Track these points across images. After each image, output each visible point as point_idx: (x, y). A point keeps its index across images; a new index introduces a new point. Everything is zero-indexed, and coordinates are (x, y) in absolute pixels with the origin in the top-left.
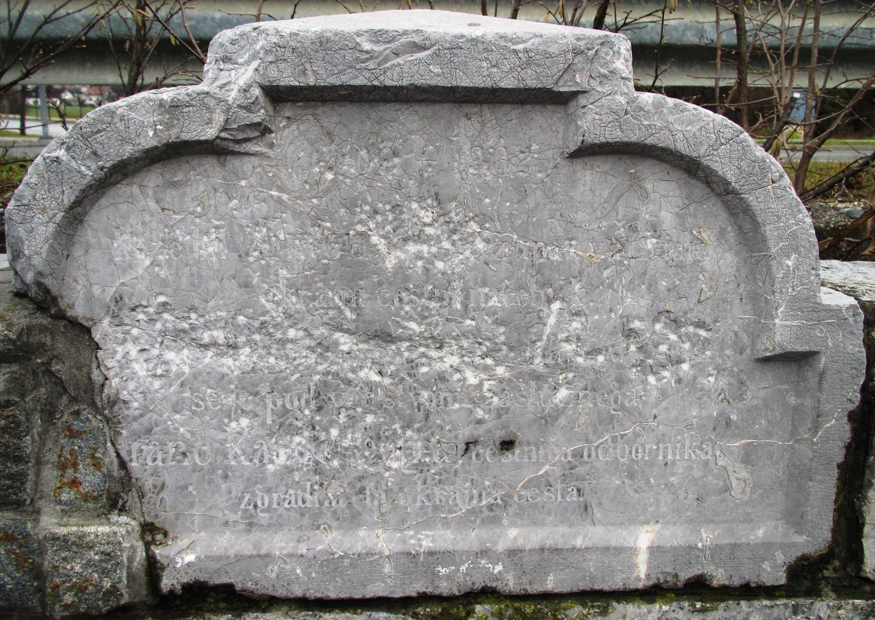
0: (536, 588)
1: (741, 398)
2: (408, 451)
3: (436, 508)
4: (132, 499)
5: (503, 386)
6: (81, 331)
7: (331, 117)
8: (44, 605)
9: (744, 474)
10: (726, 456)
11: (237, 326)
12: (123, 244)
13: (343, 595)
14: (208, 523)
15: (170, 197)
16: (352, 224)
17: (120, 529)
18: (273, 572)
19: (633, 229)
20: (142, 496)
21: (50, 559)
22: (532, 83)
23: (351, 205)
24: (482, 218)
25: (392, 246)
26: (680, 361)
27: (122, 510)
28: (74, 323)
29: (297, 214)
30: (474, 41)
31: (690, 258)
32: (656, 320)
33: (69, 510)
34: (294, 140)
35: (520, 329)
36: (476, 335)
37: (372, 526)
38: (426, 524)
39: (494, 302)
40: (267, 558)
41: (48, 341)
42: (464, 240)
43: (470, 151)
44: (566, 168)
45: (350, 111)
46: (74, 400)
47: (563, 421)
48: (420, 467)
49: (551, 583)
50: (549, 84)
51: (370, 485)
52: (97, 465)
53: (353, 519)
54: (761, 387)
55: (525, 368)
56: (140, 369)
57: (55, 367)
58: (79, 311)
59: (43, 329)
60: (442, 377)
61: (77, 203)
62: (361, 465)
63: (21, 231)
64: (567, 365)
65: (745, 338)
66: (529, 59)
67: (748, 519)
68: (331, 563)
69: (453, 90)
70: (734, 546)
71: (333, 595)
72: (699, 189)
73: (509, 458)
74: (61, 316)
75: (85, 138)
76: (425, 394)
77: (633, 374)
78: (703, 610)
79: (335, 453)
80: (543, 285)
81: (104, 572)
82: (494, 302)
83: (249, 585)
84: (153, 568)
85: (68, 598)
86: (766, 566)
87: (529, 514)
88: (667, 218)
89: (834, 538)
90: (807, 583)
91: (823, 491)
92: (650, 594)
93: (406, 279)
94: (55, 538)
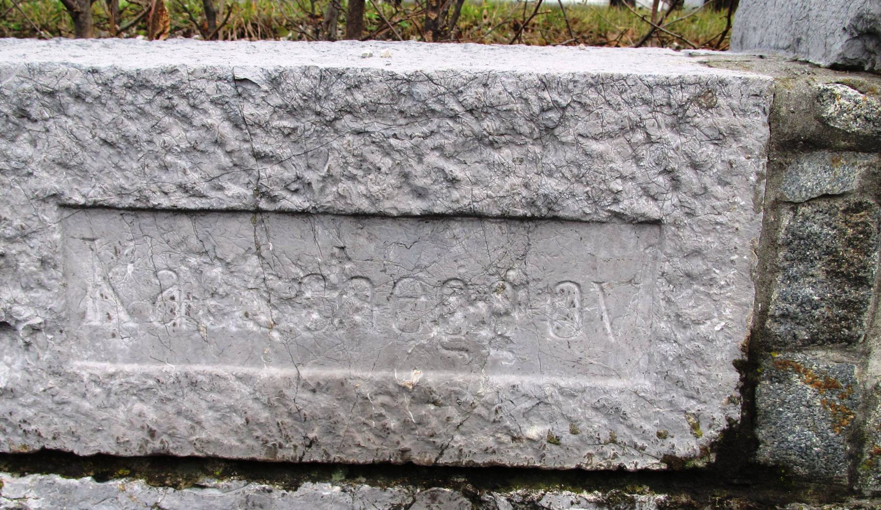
8: (853, 476)
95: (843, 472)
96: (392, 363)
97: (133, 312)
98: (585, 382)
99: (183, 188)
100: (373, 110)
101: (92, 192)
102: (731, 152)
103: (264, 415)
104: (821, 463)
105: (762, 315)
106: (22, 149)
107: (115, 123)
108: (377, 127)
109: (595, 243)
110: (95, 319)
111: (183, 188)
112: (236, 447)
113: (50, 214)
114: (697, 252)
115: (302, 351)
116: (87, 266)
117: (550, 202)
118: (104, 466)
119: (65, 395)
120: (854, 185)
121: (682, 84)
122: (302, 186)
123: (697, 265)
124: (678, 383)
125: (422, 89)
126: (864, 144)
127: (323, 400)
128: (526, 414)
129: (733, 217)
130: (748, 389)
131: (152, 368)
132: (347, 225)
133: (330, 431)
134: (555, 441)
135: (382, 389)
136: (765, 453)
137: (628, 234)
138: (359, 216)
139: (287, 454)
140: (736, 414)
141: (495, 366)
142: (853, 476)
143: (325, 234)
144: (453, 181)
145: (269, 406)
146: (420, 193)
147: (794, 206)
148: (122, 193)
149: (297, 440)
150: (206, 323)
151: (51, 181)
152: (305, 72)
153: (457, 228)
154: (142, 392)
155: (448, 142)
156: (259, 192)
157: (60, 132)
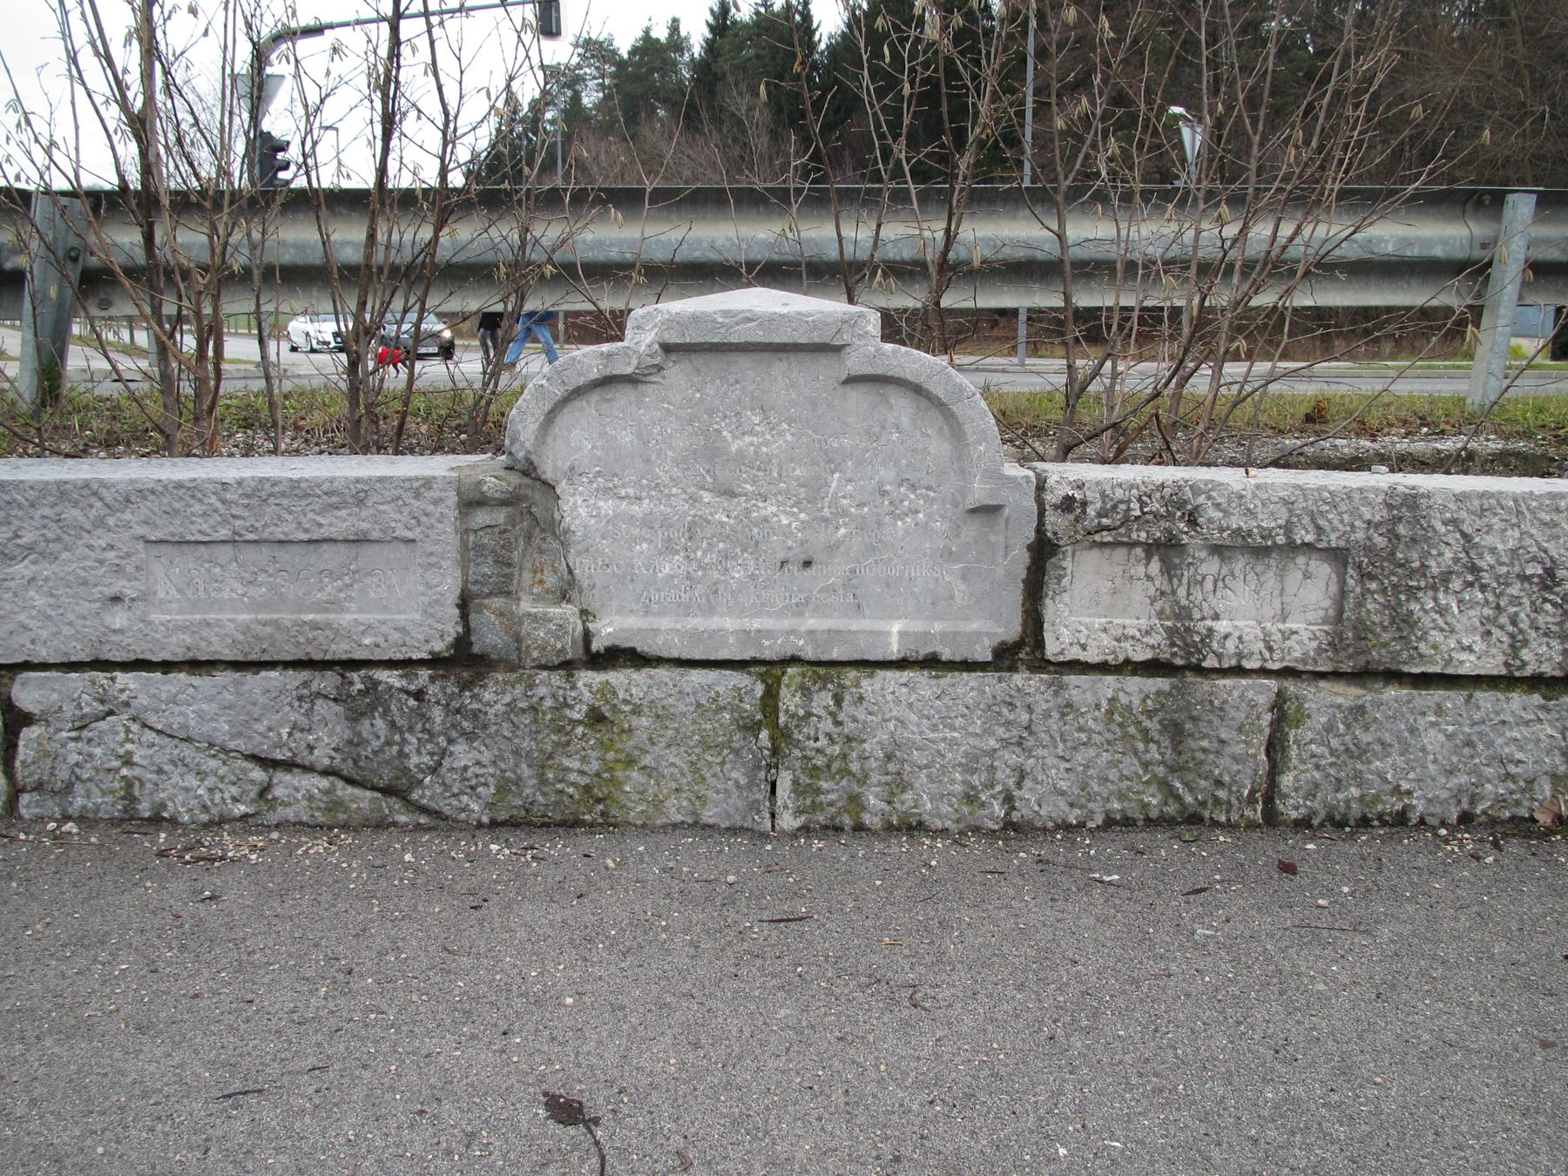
0: (825, 658)
1: (958, 536)
2: (744, 566)
3: (763, 604)
4: (574, 594)
5: (804, 526)
6: (549, 487)
7: (699, 360)
8: (520, 659)
9: (963, 587)
10: (950, 575)
11: (641, 486)
12: (576, 435)
13: (704, 657)
14: (621, 611)
15: (604, 407)
16: (711, 425)
17: (568, 611)
18: (660, 640)
19: (883, 427)
20: (581, 592)
21: (526, 627)
22: (817, 340)
23: (711, 412)
24: (790, 420)
25: (734, 437)
26: (917, 512)
27: (568, 601)
28: (545, 483)
29: (678, 418)
30: (783, 316)
31: (921, 445)
32: (900, 485)
33: (538, 599)
34: (677, 374)
35: (815, 490)
36: (787, 494)
37: (721, 616)
38: (756, 615)
39: (798, 472)
40: (656, 631)
41: (529, 492)
42: (780, 434)
43: (782, 380)
44: (841, 390)
45: (709, 357)
46: (543, 530)
47: (842, 549)
48: (752, 577)
49: (835, 654)
50: (827, 340)
51: (721, 588)
52: (555, 571)
53: (710, 610)
54: (971, 529)
55: (818, 514)
56: (583, 511)
57: (534, 510)
58: (548, 475)
59: (528, 486)
60: (766, 519)
61: (552, 411)
62: (716, 575)
63: (519, 426)
64: (845, 513)
65: (959, 498)
66: (815, 326)
67: (967, 618)
68: (696, 636)
69: (770, 344)
70: (955, 633)
71: (697, 657)
72: (924, 403)
73: (808, 573)
74: (538, 479)
75: (558, 373)
76: (756, 530)
77: (887, 519)
78: (937, 677)
79: (700, 567)
80: (830, 461)
81: (558, 638)
82: (798, 472)
83: (646, 649)
84: (587, 636)
85: (535, 654)
86: (977, 647)
87: (821, 610)
88: (905, 421)
89: (1024, 631)
90: (1008, 663)
91: (1014, 597)
92: (902, 664)
93: (744, 457)
94: (529, 615)
95: (514, 656)
96: (300, 611)
97: (180, 591)
98: (389, 617)
99: (200, 532)
100: (283, 494)
101: (160, 535)
102: (441, 508)
103: (241, 638)
104: (503, 653)
105: (466, 582)
106: (128, 516)
107: (169, 504)
108: (285, 502)
109: (387, 551)
110: (161, 595)
111: (200, 532)
112: (228, 655)
113: (140, 546)
114: (431, 554)
115: (259, 607)
116: (158, 569)
117: (365, 533)
118: (167, 666)
119: (147, 631)
120: (501, 520)
121: (417, 479)
122: (253, 529)
123: (433, 560)
124: (432, 615)
125: (303, 485)
126: (504, 503)
127: (269, 630)
128: (363, 633)
129: (446, 537)
130: (464, 617)
131: (188, 617)
132: (275, 546)
133: (272, 645)
134: (377, 646)
135: (295, 624)
136: (476, 649)
137: (402, 546)
138: (280, 542)
139: (253, 657)
140: (976, 263)
141: (348, 610)
142: (520, 659)
143: (266, 550)
144: (320, 525)
145: (243, 633)
146: (306, 531)
147: (476, 531)
148: (173, 535)
149: (257, 650)
150: (214, 594)
151: (140, 530)
152: (253, 478)
153: (325, 546)
154: (183, 629)
155: (317, 507)
156: (235, 533)
157: (144, 509)
